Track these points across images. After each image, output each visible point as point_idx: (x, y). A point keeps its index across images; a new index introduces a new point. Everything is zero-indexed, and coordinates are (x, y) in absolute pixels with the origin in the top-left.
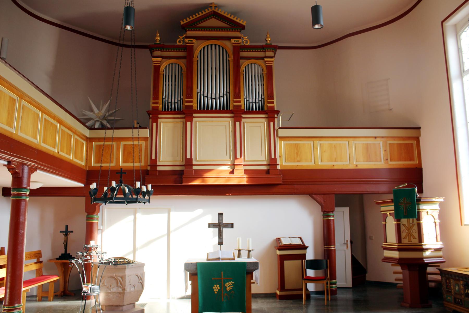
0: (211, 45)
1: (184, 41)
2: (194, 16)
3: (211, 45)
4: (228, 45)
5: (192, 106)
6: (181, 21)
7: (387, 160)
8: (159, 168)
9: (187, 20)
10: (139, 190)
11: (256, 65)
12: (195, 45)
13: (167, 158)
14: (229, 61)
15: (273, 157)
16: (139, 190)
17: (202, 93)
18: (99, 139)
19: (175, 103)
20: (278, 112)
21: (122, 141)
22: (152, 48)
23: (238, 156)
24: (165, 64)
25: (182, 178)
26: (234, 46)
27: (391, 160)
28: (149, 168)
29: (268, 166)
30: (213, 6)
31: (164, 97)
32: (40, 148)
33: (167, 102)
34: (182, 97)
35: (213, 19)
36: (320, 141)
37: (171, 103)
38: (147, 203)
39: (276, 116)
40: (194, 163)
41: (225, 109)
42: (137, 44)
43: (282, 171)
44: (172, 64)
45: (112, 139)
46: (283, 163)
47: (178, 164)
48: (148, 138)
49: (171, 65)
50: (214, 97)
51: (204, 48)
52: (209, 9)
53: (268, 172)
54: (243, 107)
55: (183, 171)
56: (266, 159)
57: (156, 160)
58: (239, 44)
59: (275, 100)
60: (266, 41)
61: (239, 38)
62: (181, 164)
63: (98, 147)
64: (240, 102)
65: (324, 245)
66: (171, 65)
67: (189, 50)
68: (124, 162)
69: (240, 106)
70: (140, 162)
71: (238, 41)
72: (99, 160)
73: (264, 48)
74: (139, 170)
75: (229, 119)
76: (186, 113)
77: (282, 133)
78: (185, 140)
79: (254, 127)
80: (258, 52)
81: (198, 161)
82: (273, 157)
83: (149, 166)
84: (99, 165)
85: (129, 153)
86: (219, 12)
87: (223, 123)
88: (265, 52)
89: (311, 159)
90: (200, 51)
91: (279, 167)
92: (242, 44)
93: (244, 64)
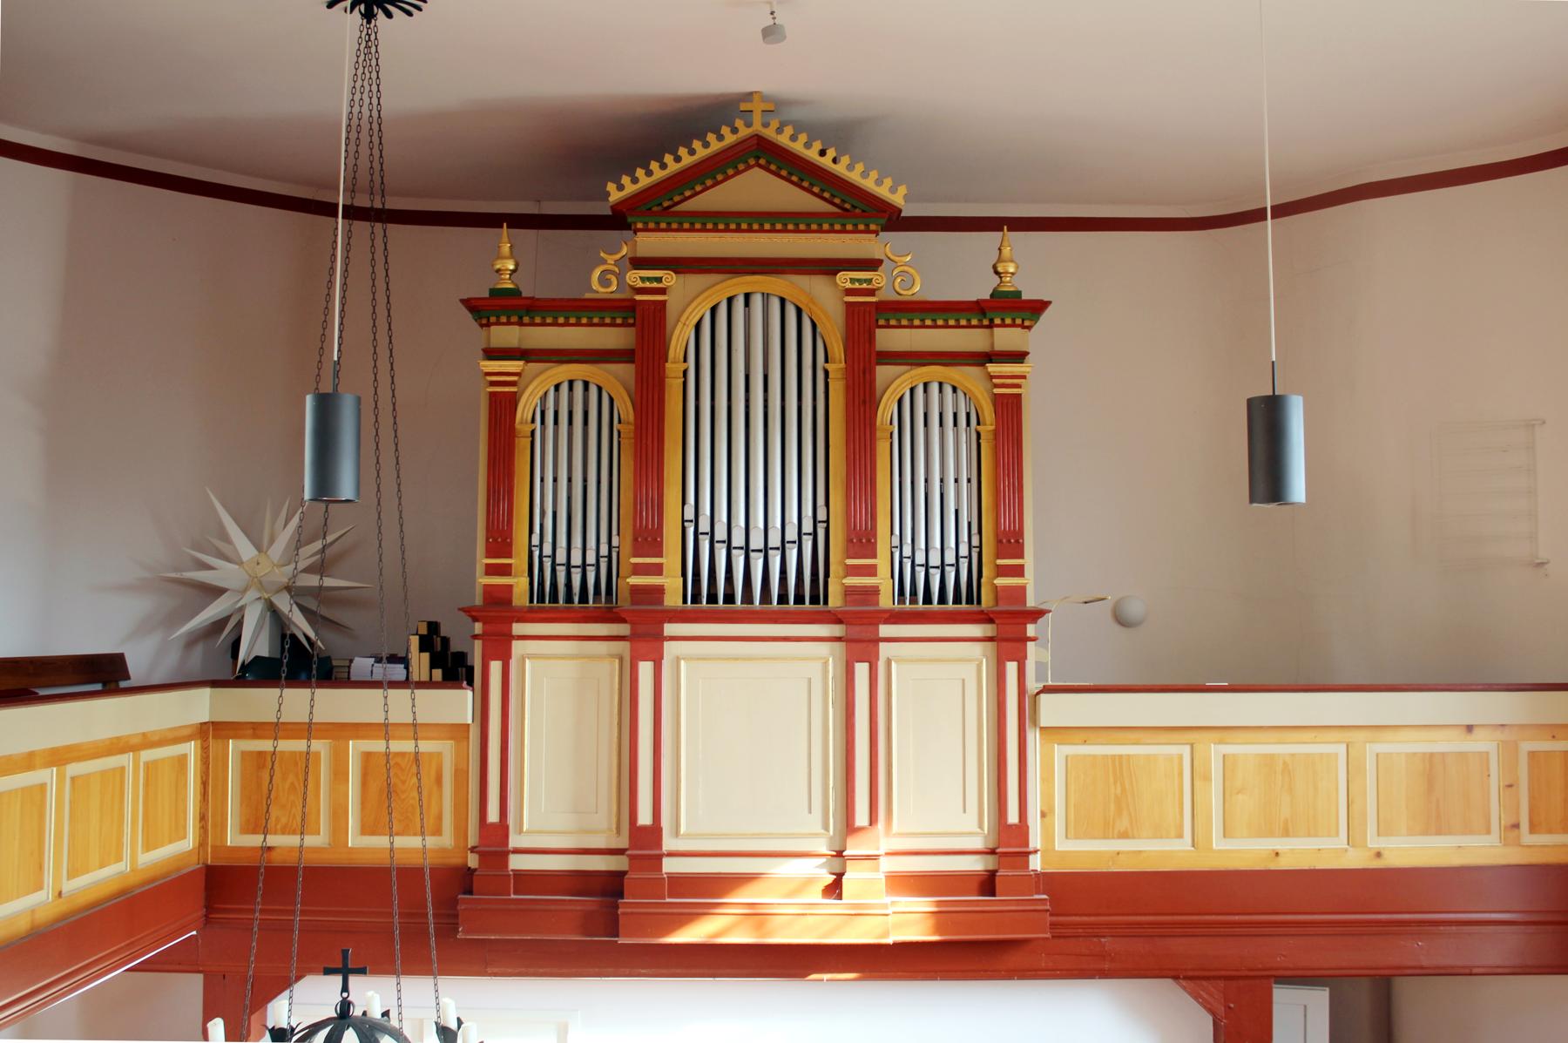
1: (620, 277)
4: (826, 298)
5: (659, 591)
6: (611, 187)
7: (1516, 826)
8: (517, 863)
12: (672, 301)
13: (553, 818)
14: (826, 373)
17: (704, 526)
18: (257, 730)
20: (1036, 615)
21: (357, 737)
23: (861, 818)
24: (536, 388)
26: (848, 304)
27: (1533, 829)
28: (473, 861)
29: (990, 858)
30: (757, 107)
33: (548, 564)
34: (615, 542)
36: (1221, 742)
37: (569, 566)
41: (805, 599)
45: (308, 730)
46: (1057, 845)
50: (757, 542)
52: (739, 123)
53: (988, 884)
55: (622, 874)
56: (981, 826)
58: (871, 292)
59: (1028, 561)
61: (872, 264)
62: (614, 845)
63: (258, 761)
65: (1019, 396)
67: (646, 320)
68: (367, 829)
69: (874, 592)
71: (869, 281)
72: (257, 822)
75: (824, 648)
76: (638, 622)
77: (1054, 710)
79: (936, 682)
81: (688, 836)
82: (1013, 817)
83: (473, 850)
84: (255, 840)
85: (389, 791)
88: (991, 326)
89: (1181, 826)
90: (698, 327)
91: (1036, 863)
92: (885, 295)
93: (894, 382)
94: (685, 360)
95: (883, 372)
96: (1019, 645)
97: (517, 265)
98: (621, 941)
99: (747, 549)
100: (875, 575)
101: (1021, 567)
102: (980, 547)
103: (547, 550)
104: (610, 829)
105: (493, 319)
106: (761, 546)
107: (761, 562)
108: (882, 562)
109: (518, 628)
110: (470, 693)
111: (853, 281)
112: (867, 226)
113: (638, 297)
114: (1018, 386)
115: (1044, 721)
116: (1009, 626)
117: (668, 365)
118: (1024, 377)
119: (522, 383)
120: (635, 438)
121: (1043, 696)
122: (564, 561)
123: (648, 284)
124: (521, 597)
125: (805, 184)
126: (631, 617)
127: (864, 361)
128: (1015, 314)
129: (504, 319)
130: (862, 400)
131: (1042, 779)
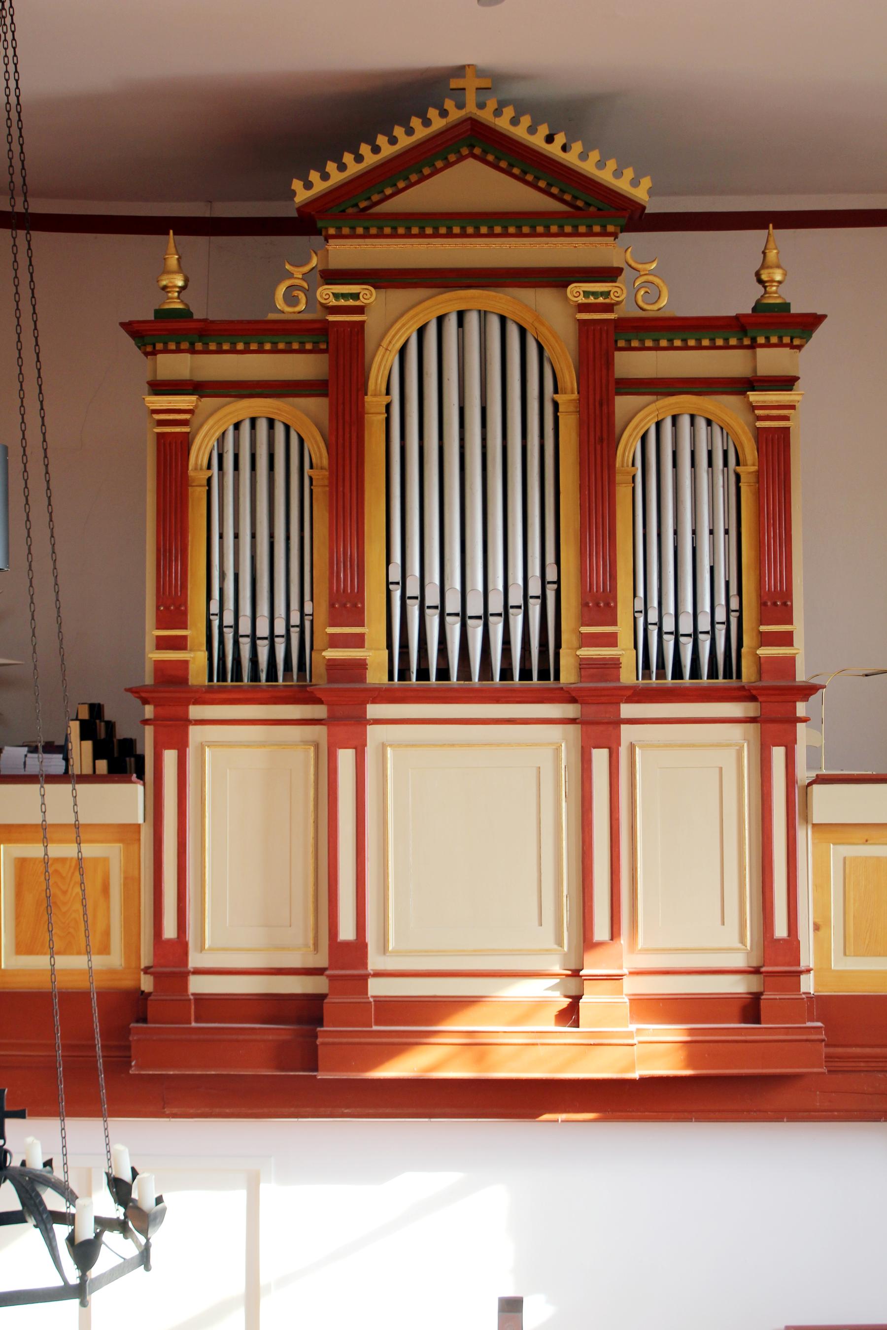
1: (310, 294)
4: (554, 315)
5: (361, 666)
8: (198, 985)
12: (372, 321)
13: (241, 933)
14: (556, 405)
15: (781, 930)
17: (413, 589)
20: (807, 691)
23: (601, 931)
24: (213, 427)
26: (582, 323)
28: (147, 984)
30: (470, 84)
31: (215, 608)
34: (308, 609)
35: (471, 164)
41: (532, 674)
42: (38, 206)
43: (823, 1005)
48: (139, 825)
50: (475, 607)
52: (449, 104)
53: (751, 1009)
55: (321, 997)
56: (742, 940)
59: (798, 627)
61: (610, 274)
62: (311, 963)
64: (611, 640)
67: (341, 345)
69: (614, 664)
71: (606, 294)
75: (555, 732)
76: (337, 702)
78: (332, 850)
79: (688, 771)
80: (714, 347)
81: (398, 953)
82: (781, 930)
83: (146, 970)
87: (532, 746)
88: (753, 346)
91: (808, 985)
93: (637, 416)
94: (388, 393)
95: (623, 404)
97: (186, 280)
100: (614, 644)
103: (229, 619)
104: (306, 945)
105: (159, 346)
107: (479, 631)
108: (623, 629)
109: (196, 711)
111: (587, 294)
113: (331, 318)
114: (786, 418)
115: (819, 815)
116: (775, 704)
118: (793, 407)
119: (196, 422)
120: (330, 485)
121: (815, 787)
123: (342, 302)
124: (198, 674)
126: (332, 700)
127: (600, 389)
129: (172, 346)
130: (599, 438)
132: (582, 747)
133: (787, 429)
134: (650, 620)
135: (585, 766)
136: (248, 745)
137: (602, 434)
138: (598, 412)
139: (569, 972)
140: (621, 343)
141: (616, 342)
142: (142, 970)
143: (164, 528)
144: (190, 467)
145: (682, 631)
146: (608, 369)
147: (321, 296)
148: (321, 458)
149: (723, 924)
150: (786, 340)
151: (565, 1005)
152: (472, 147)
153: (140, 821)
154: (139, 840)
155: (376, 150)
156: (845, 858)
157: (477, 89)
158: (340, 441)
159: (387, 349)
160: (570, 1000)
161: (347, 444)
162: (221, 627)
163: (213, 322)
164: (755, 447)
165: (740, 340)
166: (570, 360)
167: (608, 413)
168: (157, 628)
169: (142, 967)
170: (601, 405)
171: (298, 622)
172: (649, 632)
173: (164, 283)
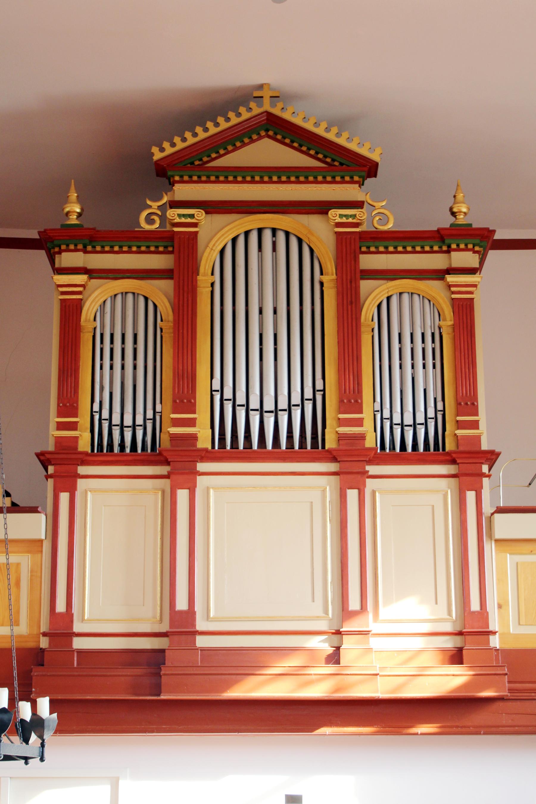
0: (260, 231)
1: (163, 218)
2: (199, 130)
3: (260, 231)
4: (320, 231)
5: (194, 438)
6: (155, 149)
8: (78, 643)
9: (173, 145)
10: (5, 717)
11: (416, 297)
13: (110, 608)
14: (322, 284)
15: (475, 606)
16: (5, 717)
17: (228, 394)
19: (134, 426)
20: (492, 457)
22: (49, 243)
23: (354, 604)
25: (158, 675)
28: (44, 643)
29: (458, 638)
30: (266, 94)
31: (96, 407)
32: (331, 698)
33: (106, 425)
34: (158, 408)
37: (122, 427)
38: (34, 762)
39: (485, 468)
40: (201, 625)
41: (310, 446)
44: (124, 294)
47: (147, 629)
48: (41, 541)
49: (119, 297)
50: (269, 405)
51: (234, 240)
52: (252, 105)
54: (371, 441)
55: (162, 651)
57: (69, 614)
58: (357, 225)
59: (482, 417)
60: (453, 214)
61: (359, 205)
64: (359, 423)
66: (119, 297)
67: (181, 247)
69: (362, 437)
70: (14, 622)
71: (354, 216)
73: (443, 239)
74: (10, 650)
77: (506, 526)
78: (173, 550)
79: (411, 505)
81: (216, 620)
82: (475, 606)
83: (45, 634)
86: (287, 116)
87: (302, 494)
88: (448, 252)
90: (222, 252)
91: (495, 642)
93: (374, 293)
94: (212, 274)
95: (365, 285)
96: (477, 478)
97: (82, 209)
98: (162, 697)
99: (261, 410)
100: (361, 425)
101: (477, 422)
102: (444, 410)
103: (105, 414)
104: (155, 617)
105: (63, 247)
106: (273, 408)
107: (272, 420)
108: (367, 415)
109: (82, 470)
110: (43, 517)
111: (341, 216)
112: (352, 178)
113: (176, 229)
115: (498, 535)
116: (469, 463)
117: (199, 278)
118: (475, 286)
119: (86, 293)
120: (174, 332)
121: (496, 515)
122: (118, 422)
123: (183, 220)
124: (84, 445)
125: (304, 149)
126: (172, 459)
128: (467, 241)
129: (72, 247)
131: (498, 580)
132: (341, 488)
133: (472, 299)
134: (384, 416)
135: (343, 500)
136: (117, 491)
137: (351, 276)
138: (349, 286)
139: (334, 631)
140: (364, 249)
141: (360, 248)
142: (41, 633)
143: (64, 359)
144: (82, 320)
145: (405, 423)
146: (355, 261)
147: (170, 215)
148: (168, 316)
149: (436, 603)
150: (470, 246)
151: (331, 652)
152: (267, 130)
153: (43, 537)
154: (42, 551)
155: (206, 130)
156: (517, 563)
157: (271, 97)
158: (181, 303)
159: (212, 249)
160: (335, 649)
161: (185, 305)
162: (100, 419)
163: (98, 231)
164: (451, 310)
165: (440, 247)
166: (331, 256)
167: (356, 287)
168: (58, 417)
169: (42, 631)
170: (351, 282)
171: (151, 417)
172: (384, 423)
173: (67, 210)
